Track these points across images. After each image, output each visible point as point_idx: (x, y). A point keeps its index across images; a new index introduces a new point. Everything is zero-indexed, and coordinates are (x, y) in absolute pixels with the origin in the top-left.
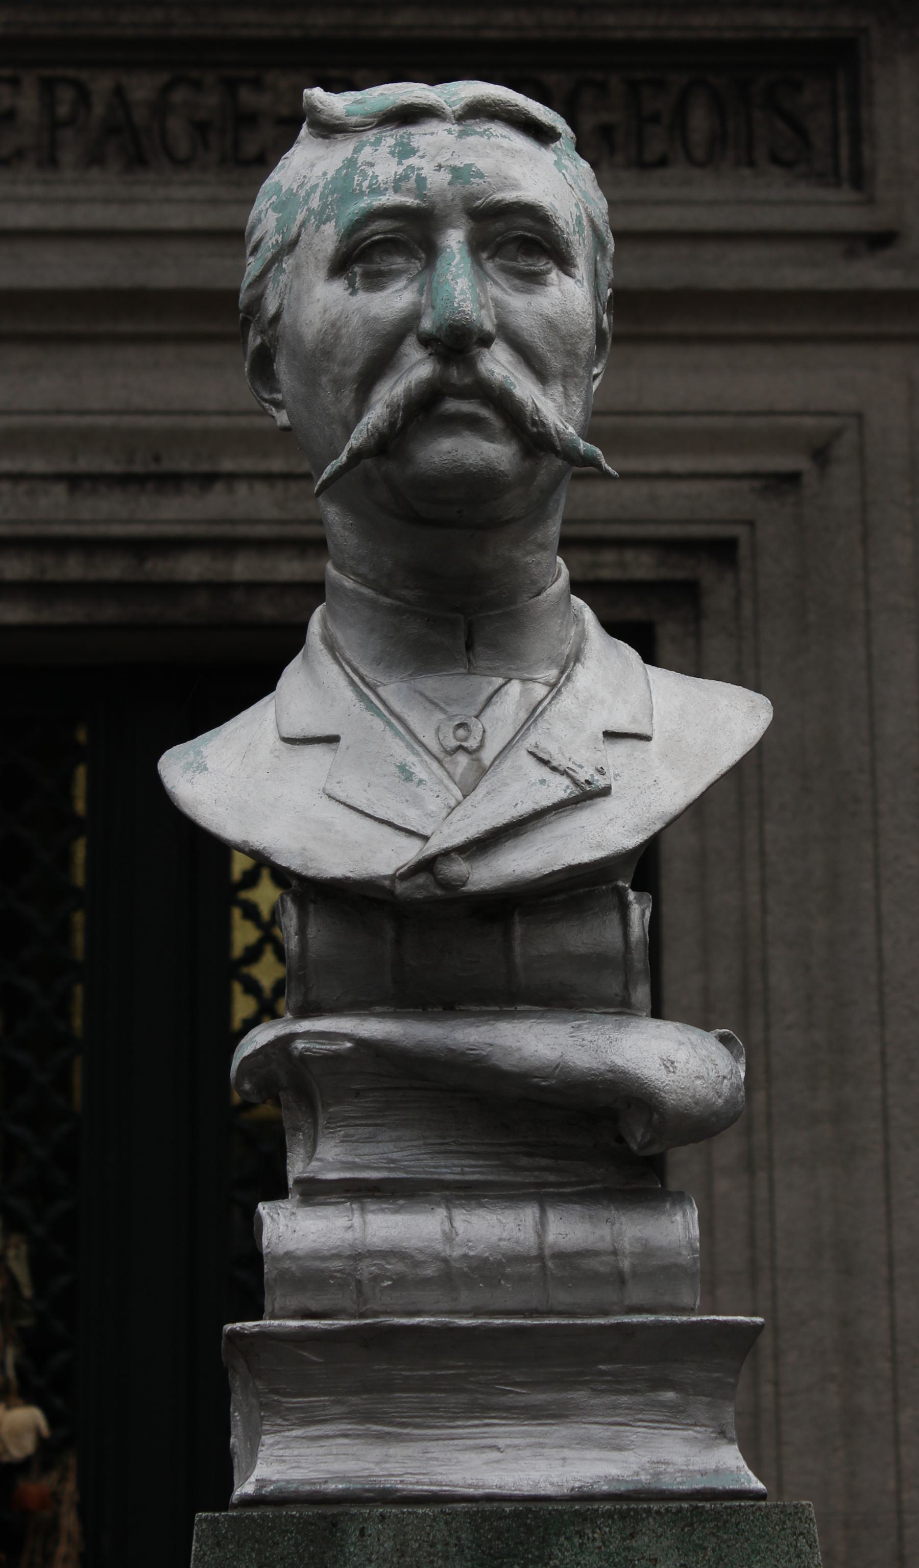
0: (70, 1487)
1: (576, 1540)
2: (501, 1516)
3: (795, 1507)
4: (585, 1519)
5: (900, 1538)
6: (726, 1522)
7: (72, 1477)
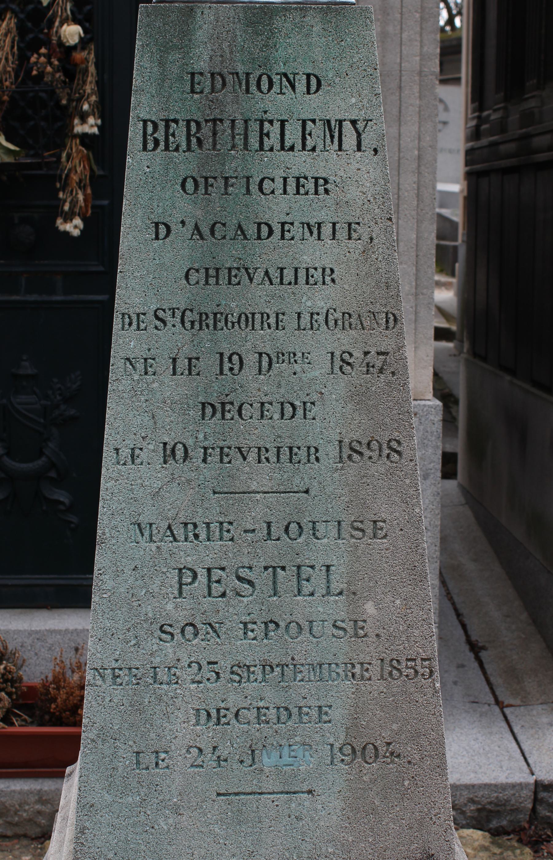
0: (92, 56)
1: (283, 18)
2: (255, 8)
3: (366, 8)
4: (287, 10)
5: (401, 80)
6: (340, 12)
7: (93, 52)
